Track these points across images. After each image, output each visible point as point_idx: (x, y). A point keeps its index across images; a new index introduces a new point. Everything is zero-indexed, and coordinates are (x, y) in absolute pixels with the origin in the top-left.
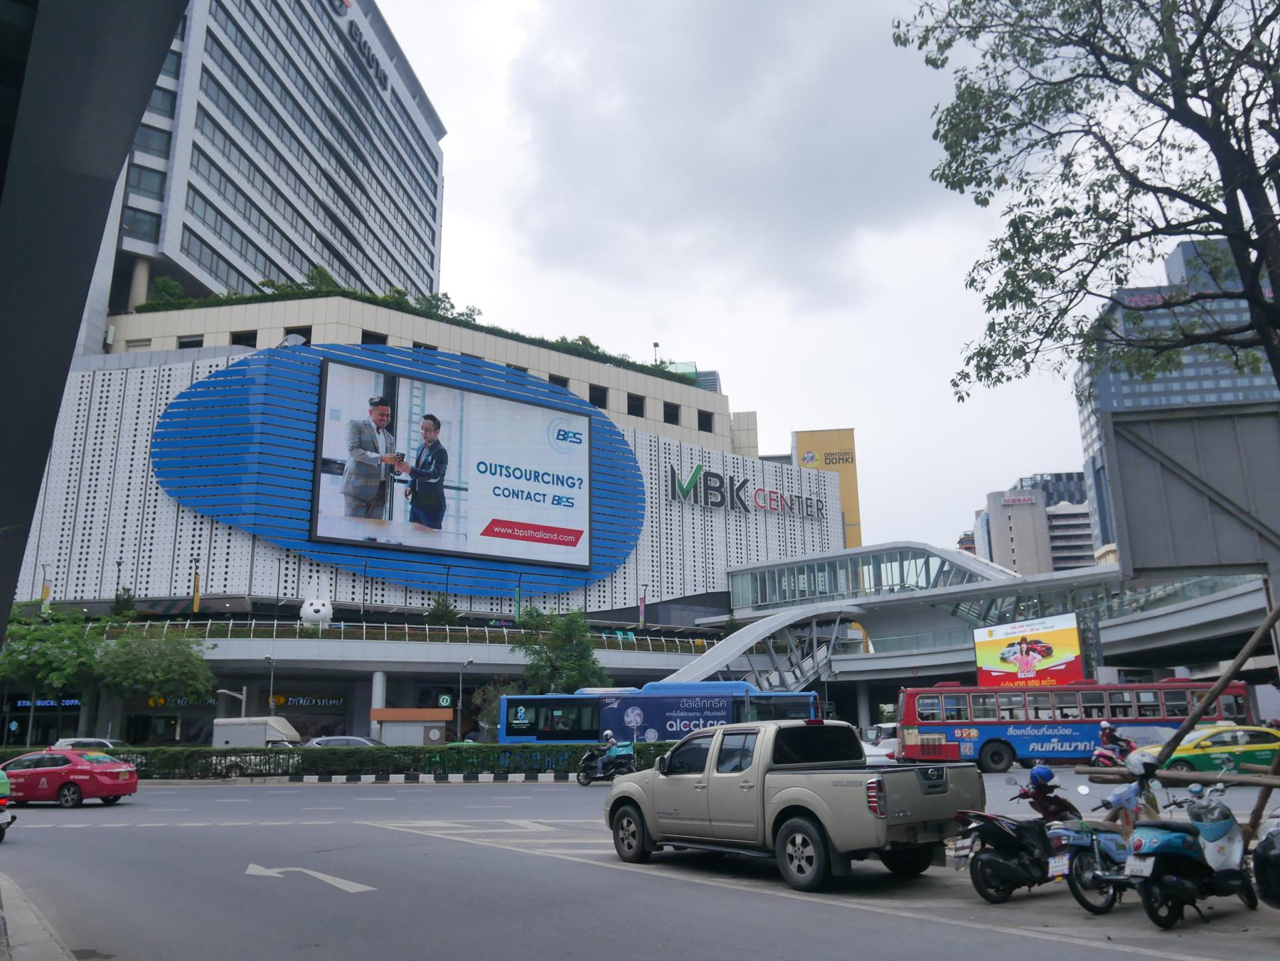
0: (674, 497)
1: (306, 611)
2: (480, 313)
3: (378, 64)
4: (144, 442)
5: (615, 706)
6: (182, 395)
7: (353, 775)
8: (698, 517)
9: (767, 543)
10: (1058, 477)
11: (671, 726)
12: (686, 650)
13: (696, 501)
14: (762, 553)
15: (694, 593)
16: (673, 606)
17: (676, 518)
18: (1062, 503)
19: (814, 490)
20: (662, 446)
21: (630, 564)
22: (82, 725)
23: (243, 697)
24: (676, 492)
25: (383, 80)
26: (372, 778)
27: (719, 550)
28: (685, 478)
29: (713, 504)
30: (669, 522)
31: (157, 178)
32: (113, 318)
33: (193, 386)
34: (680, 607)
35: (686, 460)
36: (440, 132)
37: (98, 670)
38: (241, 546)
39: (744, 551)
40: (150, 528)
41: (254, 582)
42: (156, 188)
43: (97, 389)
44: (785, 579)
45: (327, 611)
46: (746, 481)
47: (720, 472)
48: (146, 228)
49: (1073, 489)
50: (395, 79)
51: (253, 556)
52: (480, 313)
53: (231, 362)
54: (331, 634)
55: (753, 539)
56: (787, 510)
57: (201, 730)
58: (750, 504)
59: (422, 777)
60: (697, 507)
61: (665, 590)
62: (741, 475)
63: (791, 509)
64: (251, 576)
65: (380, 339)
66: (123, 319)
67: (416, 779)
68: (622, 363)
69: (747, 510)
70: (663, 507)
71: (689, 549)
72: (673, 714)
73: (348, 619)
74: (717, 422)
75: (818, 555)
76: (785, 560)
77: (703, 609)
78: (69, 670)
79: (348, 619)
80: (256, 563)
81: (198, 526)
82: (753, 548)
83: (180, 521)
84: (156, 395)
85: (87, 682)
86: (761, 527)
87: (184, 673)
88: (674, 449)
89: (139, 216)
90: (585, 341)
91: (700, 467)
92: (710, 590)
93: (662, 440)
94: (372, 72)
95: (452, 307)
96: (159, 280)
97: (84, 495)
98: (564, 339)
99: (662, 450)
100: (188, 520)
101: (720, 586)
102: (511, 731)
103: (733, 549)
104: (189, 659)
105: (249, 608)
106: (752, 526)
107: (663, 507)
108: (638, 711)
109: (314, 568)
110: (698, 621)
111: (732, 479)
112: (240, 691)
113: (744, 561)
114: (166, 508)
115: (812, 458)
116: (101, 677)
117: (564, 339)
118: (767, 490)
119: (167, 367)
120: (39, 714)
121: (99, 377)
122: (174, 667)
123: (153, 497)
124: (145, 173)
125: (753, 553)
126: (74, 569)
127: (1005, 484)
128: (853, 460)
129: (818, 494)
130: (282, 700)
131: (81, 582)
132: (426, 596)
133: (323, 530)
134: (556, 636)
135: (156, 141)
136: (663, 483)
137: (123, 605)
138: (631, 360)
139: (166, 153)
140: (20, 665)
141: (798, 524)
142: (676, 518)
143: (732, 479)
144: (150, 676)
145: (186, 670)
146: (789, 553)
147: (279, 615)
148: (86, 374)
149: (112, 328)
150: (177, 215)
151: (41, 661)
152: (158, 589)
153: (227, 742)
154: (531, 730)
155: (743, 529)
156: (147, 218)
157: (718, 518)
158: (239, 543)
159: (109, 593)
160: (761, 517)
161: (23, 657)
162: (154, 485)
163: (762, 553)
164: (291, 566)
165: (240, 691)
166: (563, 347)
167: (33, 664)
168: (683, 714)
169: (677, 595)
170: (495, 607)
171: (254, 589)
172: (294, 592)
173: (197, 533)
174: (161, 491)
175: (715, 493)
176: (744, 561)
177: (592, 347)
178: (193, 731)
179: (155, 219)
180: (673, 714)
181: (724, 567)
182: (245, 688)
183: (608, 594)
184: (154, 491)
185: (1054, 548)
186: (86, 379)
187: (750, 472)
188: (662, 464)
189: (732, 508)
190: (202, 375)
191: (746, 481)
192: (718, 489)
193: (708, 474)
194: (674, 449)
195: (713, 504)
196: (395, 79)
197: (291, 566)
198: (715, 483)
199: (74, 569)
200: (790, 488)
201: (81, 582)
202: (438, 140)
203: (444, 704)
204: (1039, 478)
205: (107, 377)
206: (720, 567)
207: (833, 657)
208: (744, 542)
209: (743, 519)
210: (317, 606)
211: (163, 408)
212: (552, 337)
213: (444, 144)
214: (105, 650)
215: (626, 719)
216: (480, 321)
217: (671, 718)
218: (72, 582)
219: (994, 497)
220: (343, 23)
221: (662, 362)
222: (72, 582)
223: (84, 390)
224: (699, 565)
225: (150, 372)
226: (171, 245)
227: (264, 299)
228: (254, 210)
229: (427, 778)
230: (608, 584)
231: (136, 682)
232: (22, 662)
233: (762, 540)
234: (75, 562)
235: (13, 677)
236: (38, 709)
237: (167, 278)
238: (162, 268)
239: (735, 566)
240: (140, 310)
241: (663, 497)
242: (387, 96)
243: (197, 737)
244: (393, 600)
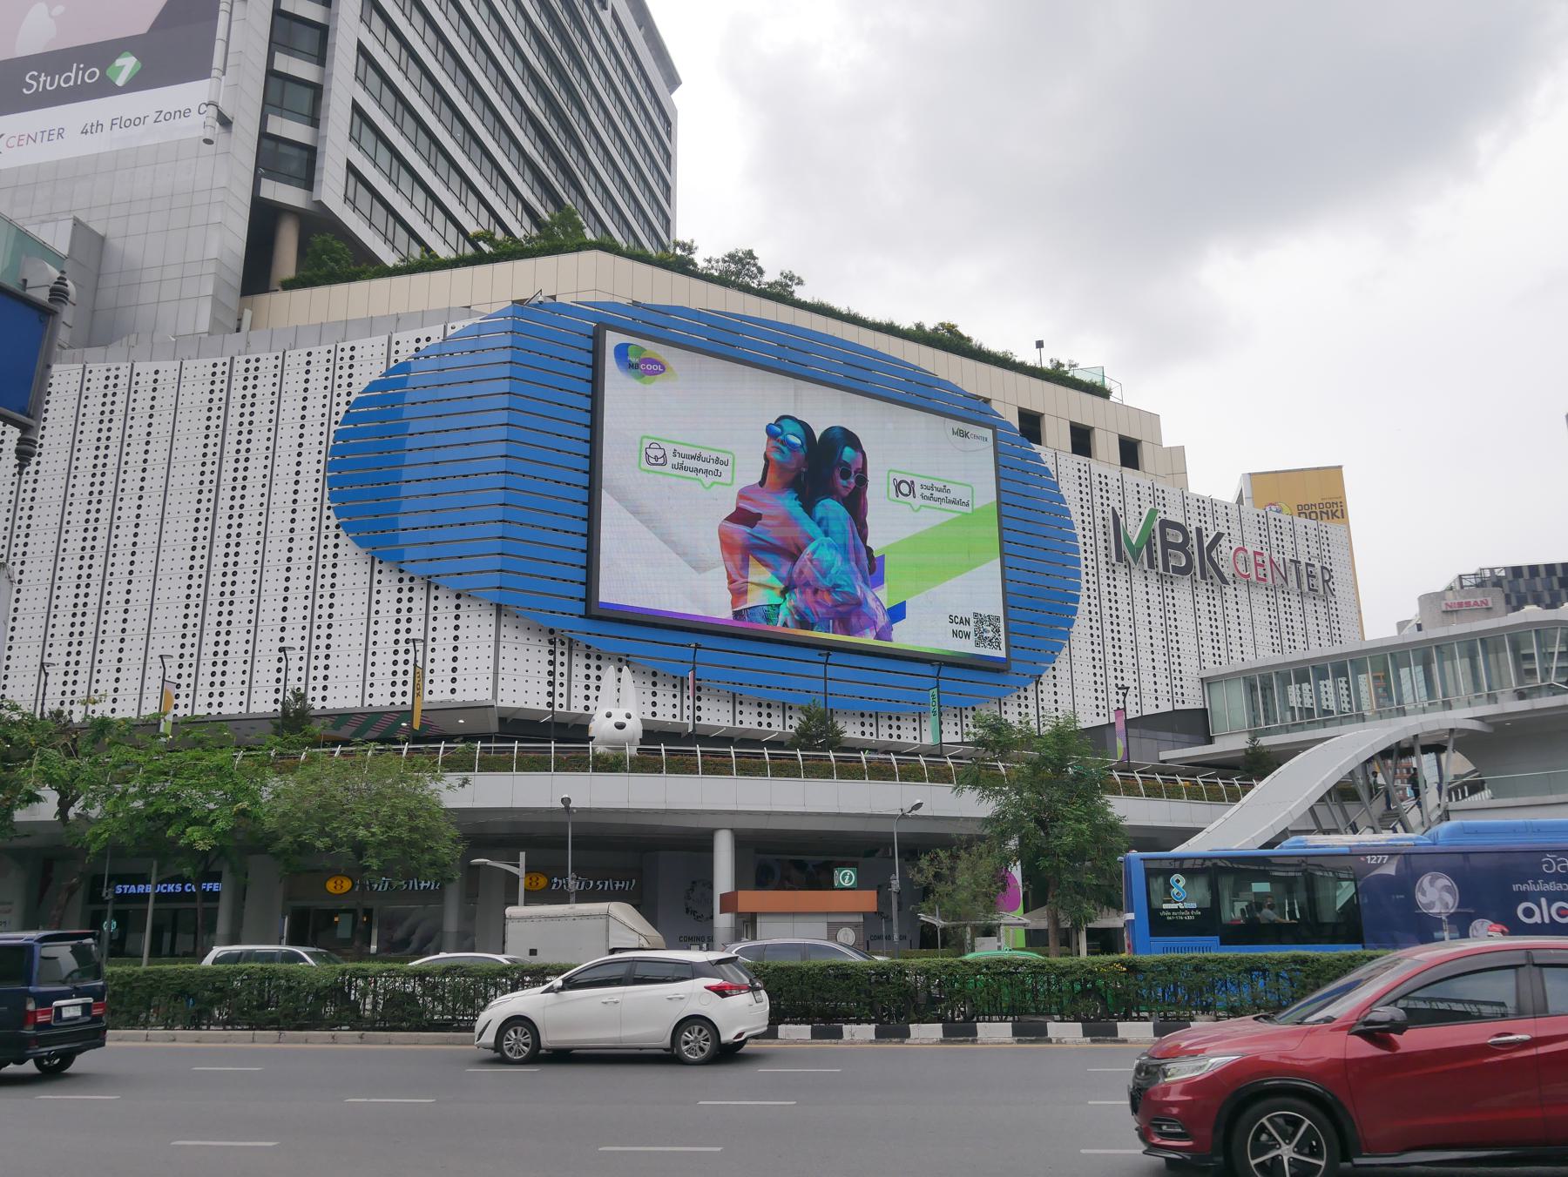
0: (1119, 559)
1: (601, 727)
2: (800, 282)
4: (313, 464)
5: (1390, 869)
6: (373, 386)
7: (892, 1027)
8: (1154, 590)
9: (1255, 634)
10: (1516, 571)
11: (1529, 913)
12: (1215, 796)
13: (1151, 565)
14: (1249, 649)
15: (1155, 711)
17: (1122, 592)
18: (1527, 608)
19: (1314, 552)
20: (1095, 478)
21: (1062, 663)
22: (223, 926)
23: (520, 871)
24: (1123, 553)
26: (867, 1031)
27: (1188, 644)
28: (1134, 531)
30: (1114, 598)
31: (308, 94)
32: (249, 298)
33: (389, 372)
35: (1131, 500)
36: (673, 81)
37: (270, 823)
38: (478, 625)
39: (1222, 645)
40: (326, 601)
41: (501, 684)
42: (306, 108)
43: (238, 384)
44: (1293, 690)
45: (634, 728)
46: (1219, 536)
47: (1181, 521)
48: (293, 167)
49: (1540, 588)
51: (497, 641)
52: (800, 282)
53: (450, 332)
54: (645, 763)
55: (1233, 626)
56: (1279, 581)
57: (411, 932)
58: (1227, 572)
59: (1054, 1028)
60: (1152, 576)
62: (1210, 527)
63: (1285, 579)
64: (496, 673)
66: (264, 299)
67: (1040, 1034)
68: (1003, 362)
69: (1225, 581)
70: (1103, 573)
71: (1143, 640)
72: (1530, 887)
73: (664, 748)
74: (1146, 453)
75: (1329, 650)
76: (1278, 659)
77: (1169, 735)
78: (221, 824)
79: (664, 748)
80: (502, 652)
82: (1235, 640)
83: (376, 586)
84: (331, 390)
85: (248, 844)
87: (413, 829)
89: (283, 149)
90: (951, 329)
91: (1153, 512)
92: (1179, 706)
95: (761, 271)
96: (317, 240)
97: (219, 551)
98: (919, 327)
99: (1096, 484)
100: (388, 583)
101: (1193, 700)
102: (1161, 925)
103: (1207, 643)
104: (429, 807)
105: (494, 727)
106: (1231, 605)
107: (1103, 573)
108: (1444, 881)
109: (593, 663)
110: (1164, 755)
111: (1199, 530)
112: (514, 861)
113: (1224, 660)
114: (352, 566)
116: (273, 837)
117: (919, 327)
118: (1250, 550)
119: (347, 346)
120: (163, 906)
121: (240, 366)
122: (401, 818)
123: (331, 551)
124: (290, 86)
125: (1236, 648)
126: (206, 669)
127: (1439, 582)
128: (1344, 515)
129: (1320, 557)
130: (543, 881)
131: (217, 689)
132: (765, 711)
133: (611, 592)
134: (1036, 766)
135: (307, 39)
136: (1100, 536)
137: (294, 720)
138: (1018, 360)
139: (321, 57)
140: (137, 816)
141: (1295, 605)
142: (1122, 592)
143: (1199, 530)
144: (362, 833)
145: (421, 823)
146: (1286, 649)
147: (556, 738)
148: (219, 361)
149: (248, 314)
150: (338, 150)
151: (169, 809)
152: (342, 695)
153: (533, 952)
154: (1206, 922)
155: (1219, 610)
156: (294, 152)
157: (1182, 592)
158: (474, 620)
159: (265, 703)
161: (139, 804)
162: (332, 531)
163: (1249, 649)
165: (514, 861)
166: (918, 336)
167: (158, 815)
168: (1552, 887)
170: (867, 729)
171: (500, 695)
172: (564, 701)
173: (405, 605)
174: (342, 541)
175: (1178, 551)
176: (1224, 660)
177: (961, 337)
178: (399, 934)
179: (305, 154)
180: (1530, 887)
181: (1195, 670)
182: (522, 855)
184: (331, 541)
186: (219, 370)
187: (1222, 522)
188: (1098, 508)
189: (1203, 577)
190: (405, 352)
191: (1219, 536)
192: (1182, 547)
193: (1165, 524)
195: (1177, 570)
198: (1175, 537)
199: (206, 669)
201: (217, 689)
202: (671, 92)
203: (846, 884)
204: (1488, 574)
205: (252, 365)
206: (1190, 671)
207: (1453, 805)
208: (1221, 631)
209: (1217, 595)
210: (619, 717)
211: (343, 408)
212: (906, 323)
213: (677, 97)
214: (274, 793)
215: (1421, 898)
216: (800, 293)
217: (1525, 896)
218: (204, 690)
219: (1428, 600)
221: (1059, 365)
222: (204, 690)
223: (217, 387)
225: (320, 354)
226: (331, 190)
227: (479, 259)
228: (399, 229)
229: (1064, 1032)
231: (337, 844)
232: (137, 809)
233: (1246, 628)
234: (207, 659)
235: (123, 839)
236: (160, 897)
237: (329, 237)
238: (317, 223)
239: (1211, 669)
240: (289, 285)
241: (1102, 558)
242: (606, 17)
243: (405, 942)
244: (716, 716)
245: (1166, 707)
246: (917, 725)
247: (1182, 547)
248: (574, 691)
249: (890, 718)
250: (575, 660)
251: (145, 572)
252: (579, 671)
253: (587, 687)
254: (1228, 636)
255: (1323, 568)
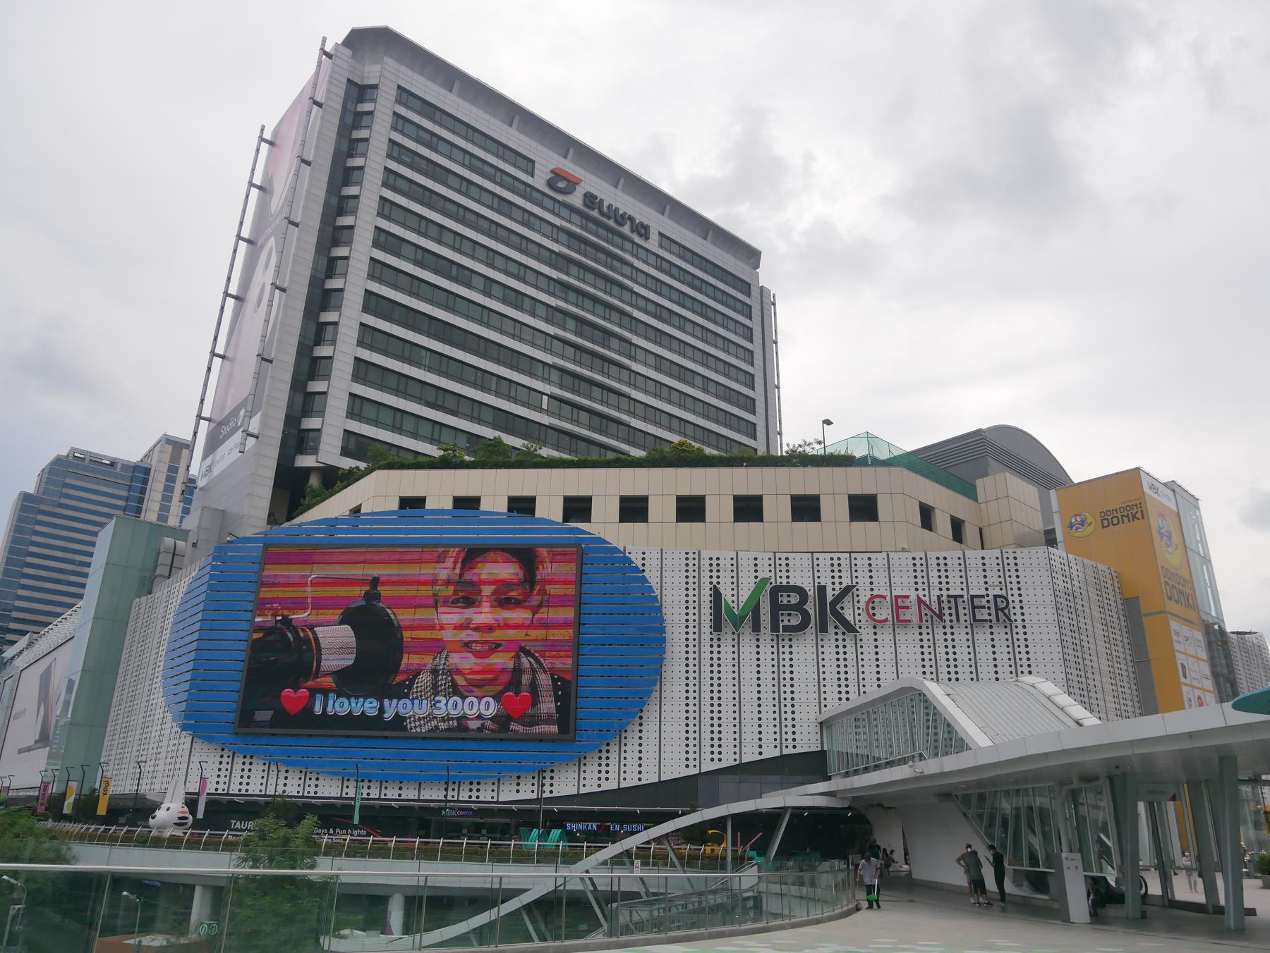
3: (631, 219)
8: (767, 650)
16: (722, 778)
25: (643, 231)
29: (786, 628)
34: (729, 777)
36: (752, 255)
50: (658, 223)
61: (707, 756)
65: (418, 502)
71: (749, 692)
77: (777, 778)
81: (247, 767)
86: (886, 653)
88: (726, 563)
92: (790, 751)
93: (705, 555)
94: (626, 230)
101: (807, 742)
106: (868, 651)
109: (247, 760)
115: (1083, 523)
157: (803, 649)
160: (885, 636)
164: (225, 759)
169: (728, 760)
183: (613, 768)
185: (1190, 706)
194: (726, 563)
196: (658, 223)
197: (225, 759)
200: (944, 583)
220: (576, 200)
224: (768, 715)
230: (613, 755)
245: (771, 752)
246: (495, 787)
247: (799, 607)
248: (703, 749)
249: (471, 783)
250: (236, 759)
251: (748, 705)
252: (238, 766)
253: (794, 740)
254: (1087, 678)
255: (920, 601)
